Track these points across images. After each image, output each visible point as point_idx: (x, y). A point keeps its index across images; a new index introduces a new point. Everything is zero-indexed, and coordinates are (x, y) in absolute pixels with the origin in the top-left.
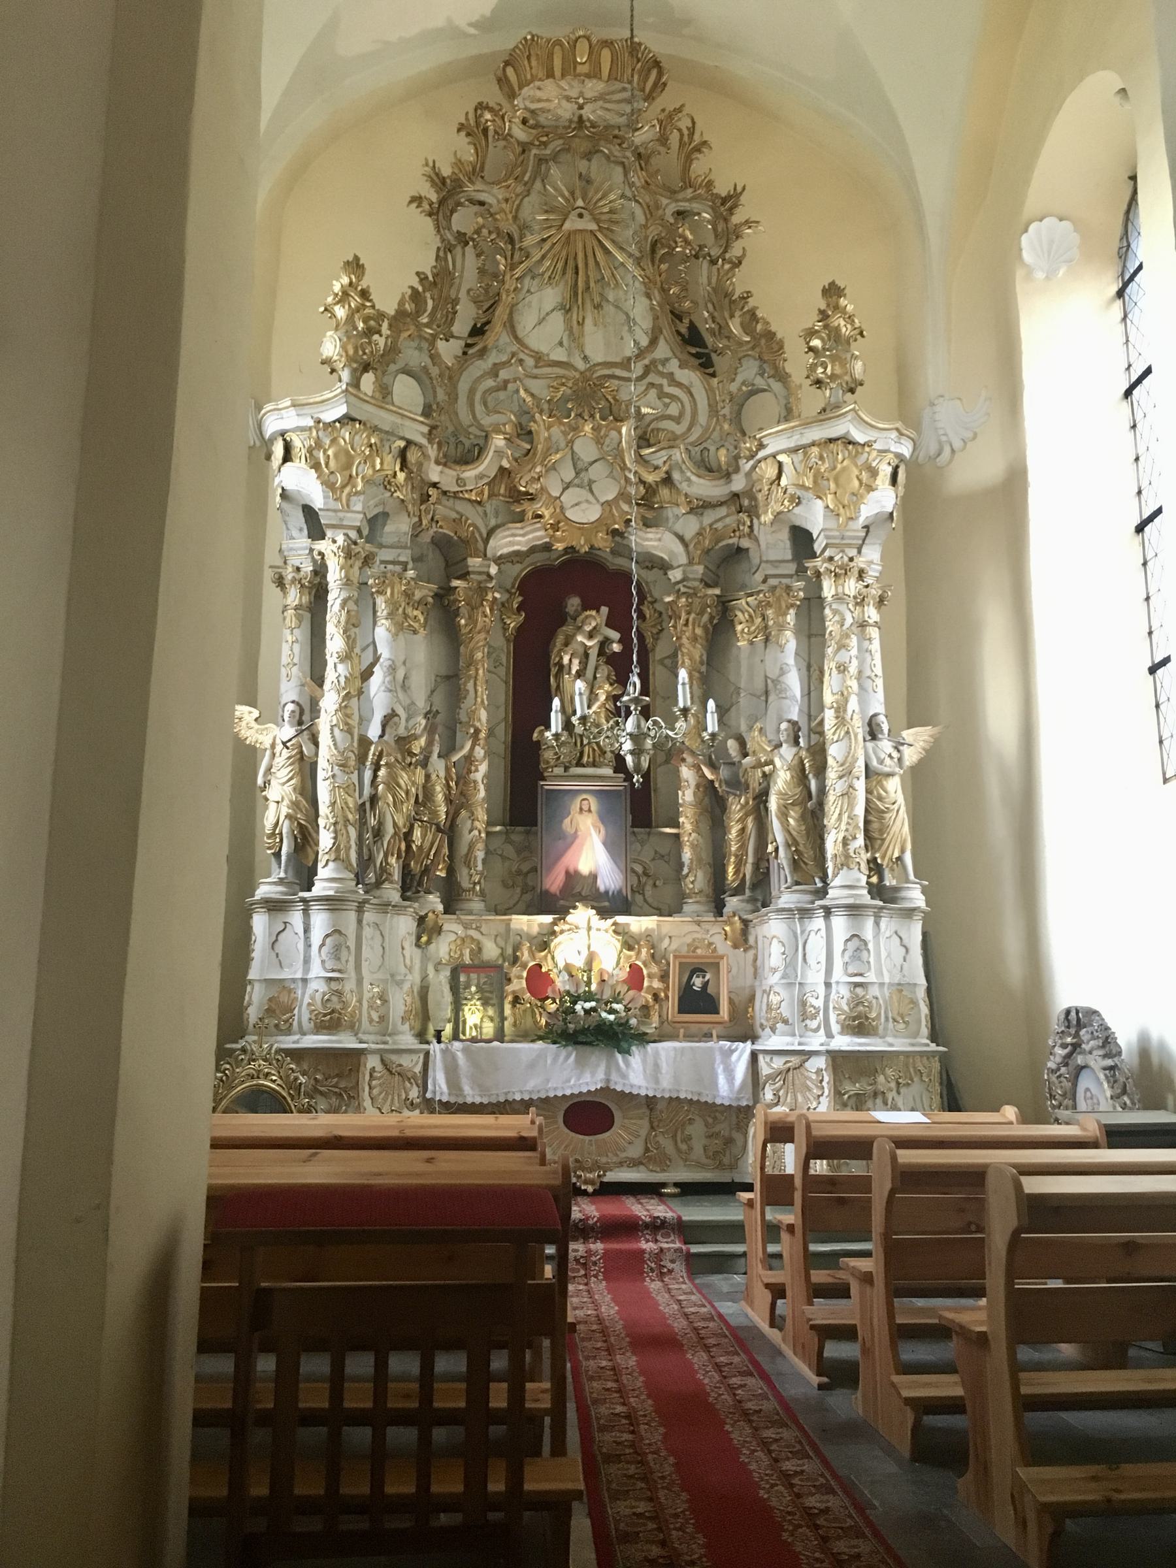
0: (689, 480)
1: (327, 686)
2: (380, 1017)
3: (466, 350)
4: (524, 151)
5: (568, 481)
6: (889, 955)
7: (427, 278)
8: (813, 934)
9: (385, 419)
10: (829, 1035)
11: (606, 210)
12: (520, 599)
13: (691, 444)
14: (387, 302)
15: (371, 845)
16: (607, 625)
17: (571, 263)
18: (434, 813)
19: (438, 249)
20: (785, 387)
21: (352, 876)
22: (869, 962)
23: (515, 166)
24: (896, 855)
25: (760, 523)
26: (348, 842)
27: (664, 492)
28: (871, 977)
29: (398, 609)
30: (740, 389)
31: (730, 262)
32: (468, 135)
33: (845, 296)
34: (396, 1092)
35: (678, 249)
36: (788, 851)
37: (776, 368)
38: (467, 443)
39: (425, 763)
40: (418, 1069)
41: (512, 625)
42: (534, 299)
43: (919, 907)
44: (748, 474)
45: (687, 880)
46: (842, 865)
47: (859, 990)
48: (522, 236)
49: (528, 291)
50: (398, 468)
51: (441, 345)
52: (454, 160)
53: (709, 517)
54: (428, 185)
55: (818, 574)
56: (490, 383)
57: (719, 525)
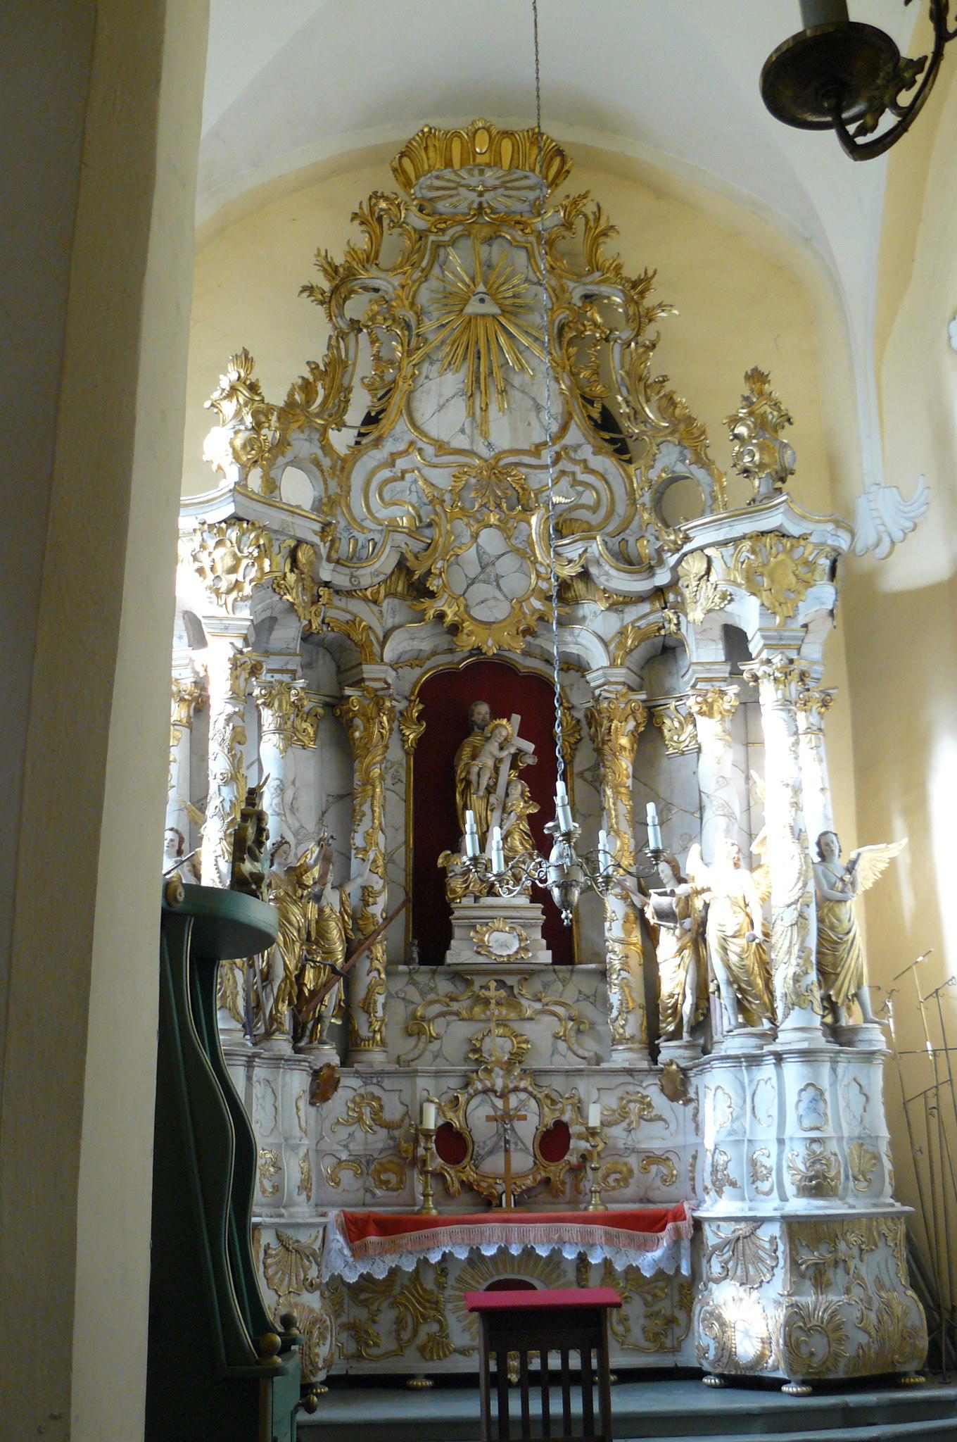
0: (607, 574)
1: (210, 811)
2: (273, 1187)
3: (359, 439)
4: (420, 238)
5: (472, 576)
6: (848, 1106)
7: (317, 367)
8: (762, 1083)
9: (273, 518)
10: (784, 1198)
11: (510, 294)
12: (421, 707)
13: (608, 535)
14: (276, 395)
15: (260, 990)
16: (518, 735)
17: (472, 350)
18: (329, 953)
19: (330, 337)
20: (709, 475)
21: (240, 1026)
22: (826, 1114)
23: (411, 253)
24: (852, 991)
25: (688, 622)
26: (236, 988)
27: (579, 587)
28: (829, 1131)
29: (286, 723)
30: (659, 477)
31: (644, 346)
32: (362, 223)
33: (769, 382)
34: (294, 1271)
35: (587, 333)
36: (730, 989)
37: (697, 454)
38: (361, 538)
39: (318, 898)
40: (317, 1246)
41: (411, 737)
42: (433, 385)
43: (880, 1050)
44: (674, 569)
45: (617, 1024)
46: (793, 1004)
47: (815, 1147)
48: (419, 323)
49: (427, 377)
50: (287, 570)
51: (333, 435)
52: (347, 249)
53: (632, 613)
54: (321, 274)
55: (756, 678)
56: (386, 473)
57: (642, 623)
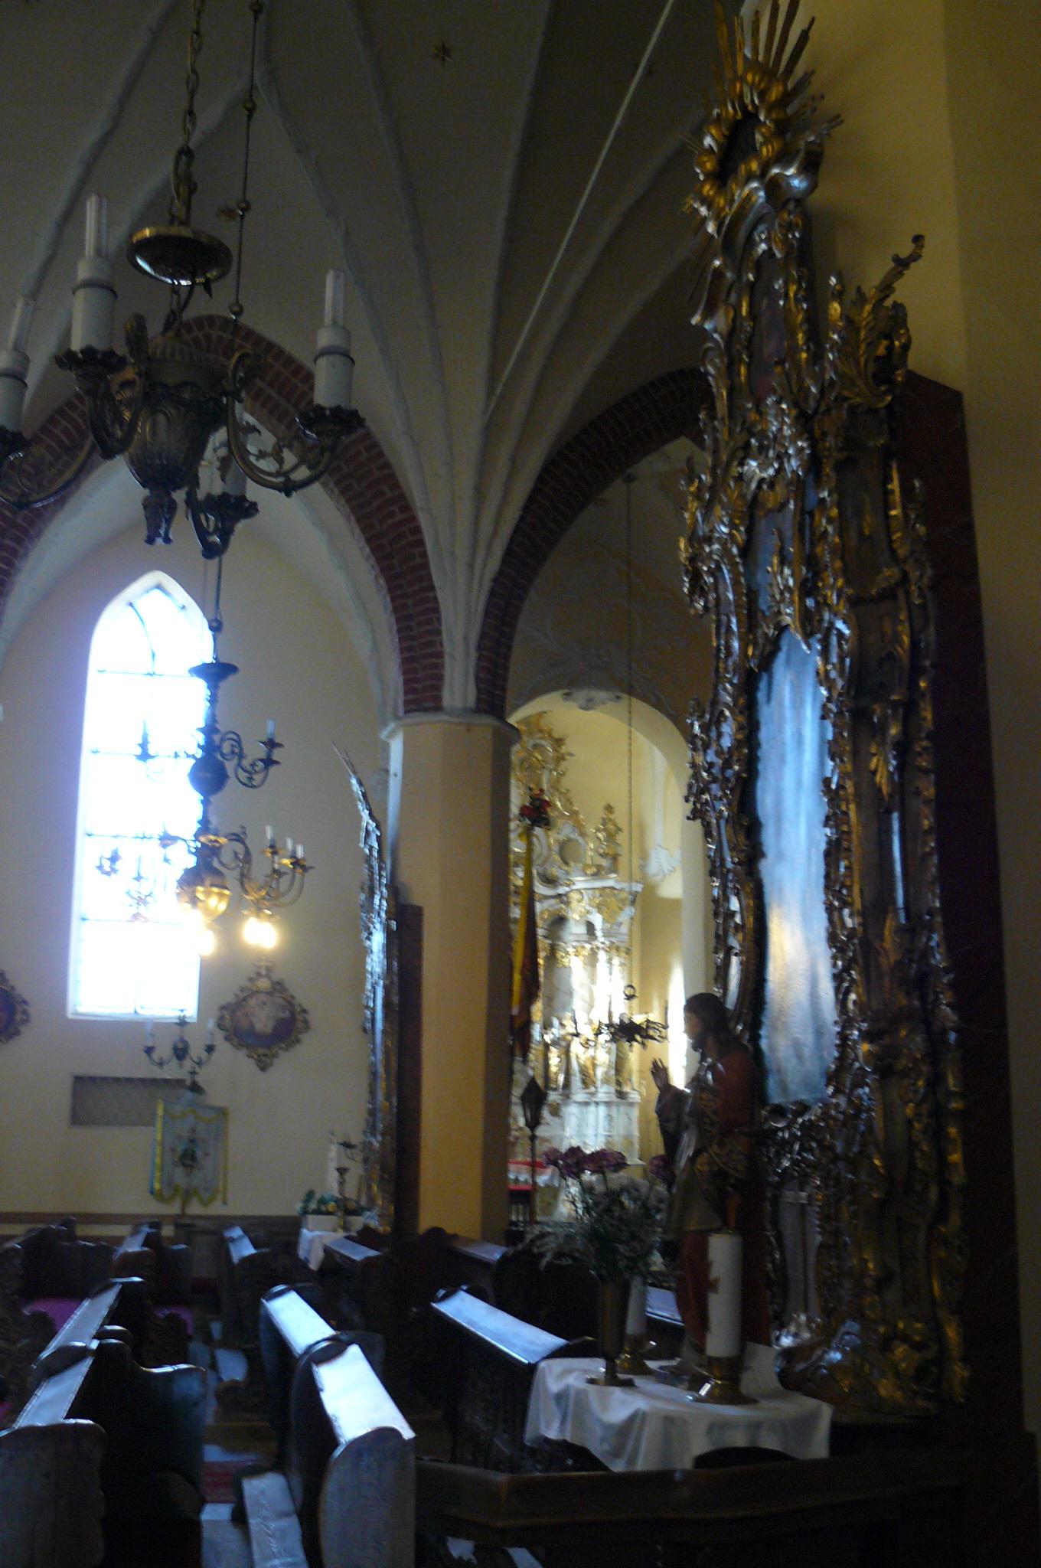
28: (615, 1133)
47: (610, 1139)
